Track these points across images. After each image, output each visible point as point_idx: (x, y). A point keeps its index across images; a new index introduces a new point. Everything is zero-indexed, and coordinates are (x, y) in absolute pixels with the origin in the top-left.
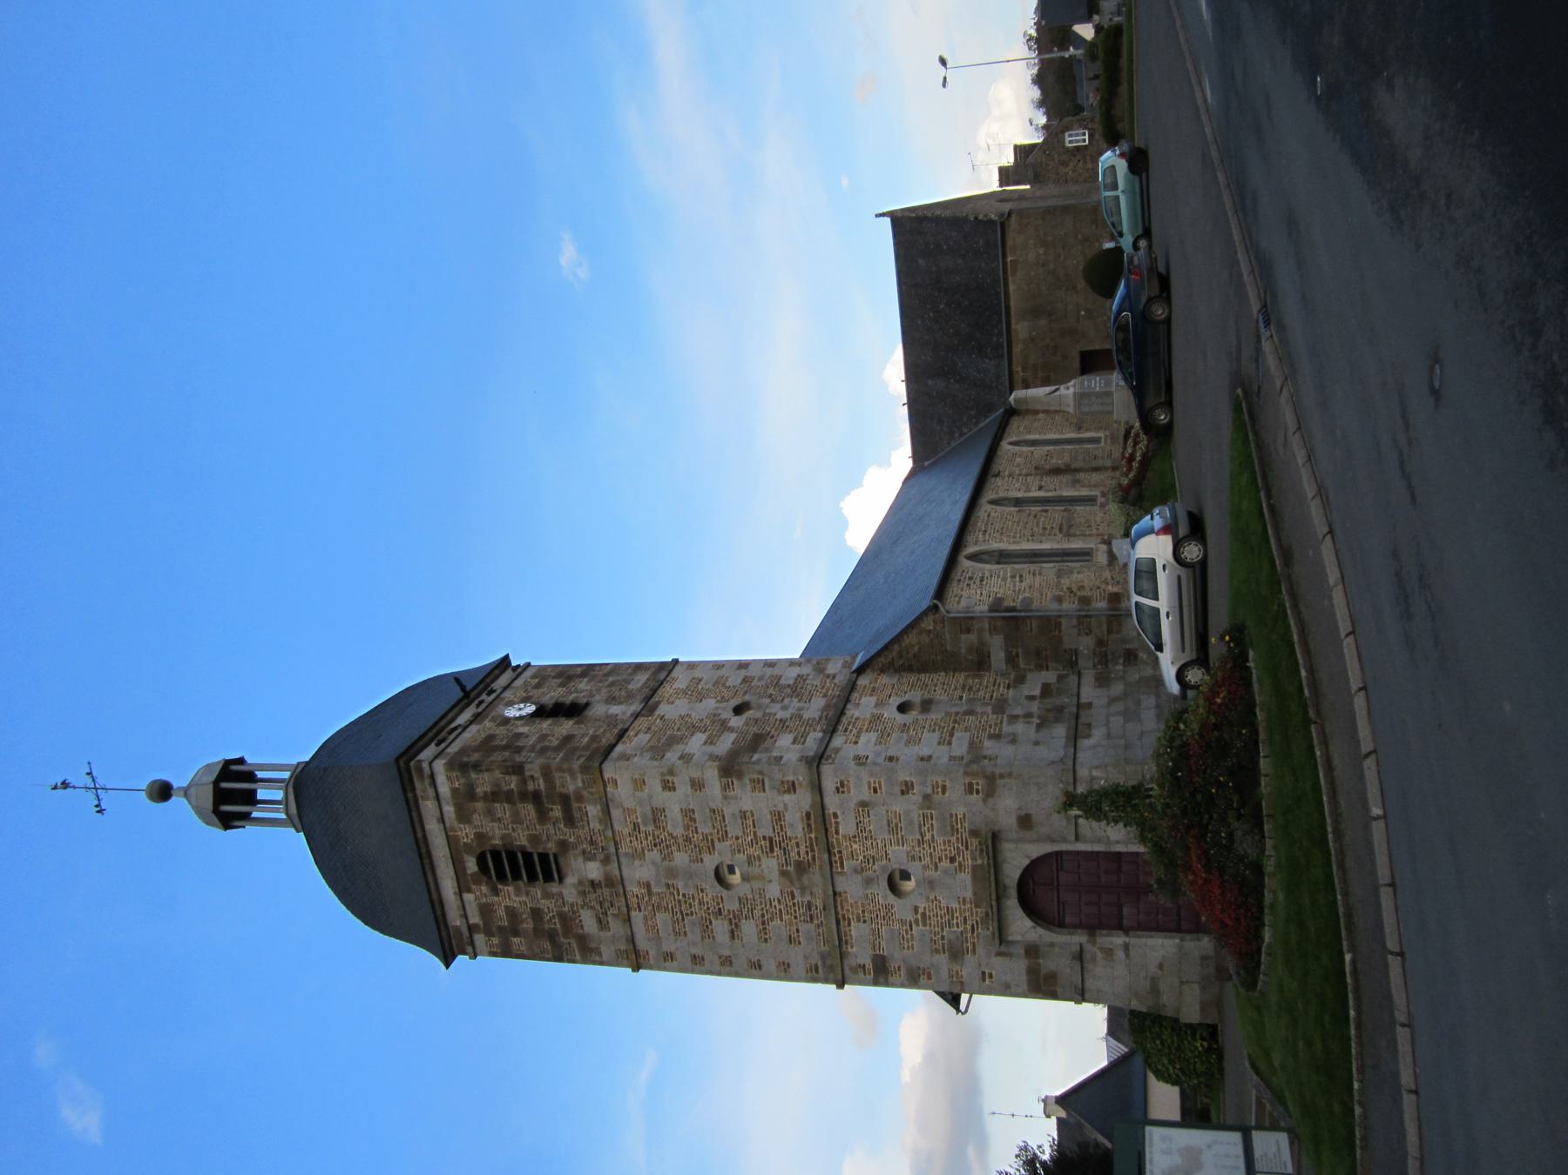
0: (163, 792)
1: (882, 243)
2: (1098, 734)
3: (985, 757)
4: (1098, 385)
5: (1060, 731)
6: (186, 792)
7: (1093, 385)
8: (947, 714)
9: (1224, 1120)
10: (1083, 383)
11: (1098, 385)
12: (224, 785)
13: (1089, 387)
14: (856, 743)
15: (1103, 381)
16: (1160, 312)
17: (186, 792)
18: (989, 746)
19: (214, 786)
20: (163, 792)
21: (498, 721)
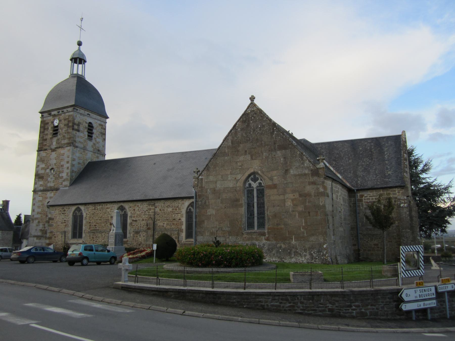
0: (80, 44)
1: (398, 133)
2: (38, 241)
3: (33, 221)
4: (111, 241)
5: (40, 234)
6: (79, 49)
7: (111, 239)
8: (47, 212)
9: (345, 283)
10: (112, 235)
11: (111, 241)
12: (78, 59)
13: (111, 238)
14: (39, 197)
15: (112, 242)
16: (64, 259)
17: (79, 49)
18: (37, 221)
19: (286, 131)
20: (80, 44)
21: (426, 214)
